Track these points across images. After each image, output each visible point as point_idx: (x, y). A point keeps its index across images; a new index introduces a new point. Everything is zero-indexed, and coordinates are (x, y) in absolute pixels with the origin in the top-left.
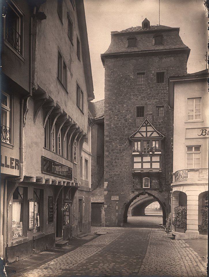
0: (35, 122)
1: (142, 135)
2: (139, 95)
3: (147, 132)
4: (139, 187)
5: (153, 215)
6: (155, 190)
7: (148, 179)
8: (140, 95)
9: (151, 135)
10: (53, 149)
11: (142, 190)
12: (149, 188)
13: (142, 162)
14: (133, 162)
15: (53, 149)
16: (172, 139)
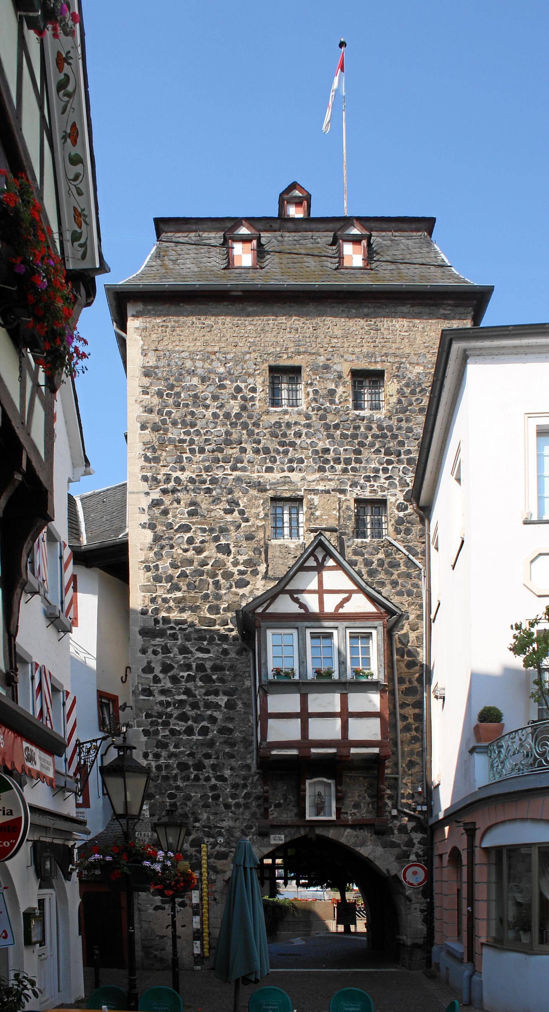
0: (439, 785)
1: (302, 606)
4: (288, 816)
6: (357, 826)
7: (329, 785)
8: (286, 453)
9: (341, 605)
11: (305, 826)
12: (334, 817)
16: (98, 872)
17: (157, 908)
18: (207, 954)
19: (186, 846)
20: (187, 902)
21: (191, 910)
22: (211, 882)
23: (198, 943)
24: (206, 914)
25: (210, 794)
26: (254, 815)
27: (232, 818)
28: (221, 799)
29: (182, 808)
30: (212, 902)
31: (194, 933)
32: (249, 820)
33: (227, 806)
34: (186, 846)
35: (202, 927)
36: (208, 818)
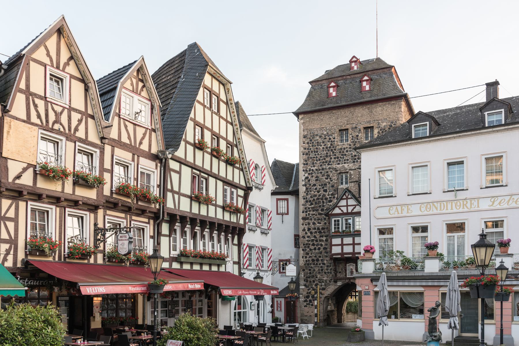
1: (342, 211)
2: (341, 157)
3: (347, 206)
5: (107, 89)
8: (343, 158)
9: (353, 210)
10: (182, 133)
13: (342, 245)
14: (331, 245)
15: (182, 133)
17: (305, 306)
19: (314, 286)
22: (320, 298)
26: (333, 275)
33: (325, 273)
34: (314, 286)
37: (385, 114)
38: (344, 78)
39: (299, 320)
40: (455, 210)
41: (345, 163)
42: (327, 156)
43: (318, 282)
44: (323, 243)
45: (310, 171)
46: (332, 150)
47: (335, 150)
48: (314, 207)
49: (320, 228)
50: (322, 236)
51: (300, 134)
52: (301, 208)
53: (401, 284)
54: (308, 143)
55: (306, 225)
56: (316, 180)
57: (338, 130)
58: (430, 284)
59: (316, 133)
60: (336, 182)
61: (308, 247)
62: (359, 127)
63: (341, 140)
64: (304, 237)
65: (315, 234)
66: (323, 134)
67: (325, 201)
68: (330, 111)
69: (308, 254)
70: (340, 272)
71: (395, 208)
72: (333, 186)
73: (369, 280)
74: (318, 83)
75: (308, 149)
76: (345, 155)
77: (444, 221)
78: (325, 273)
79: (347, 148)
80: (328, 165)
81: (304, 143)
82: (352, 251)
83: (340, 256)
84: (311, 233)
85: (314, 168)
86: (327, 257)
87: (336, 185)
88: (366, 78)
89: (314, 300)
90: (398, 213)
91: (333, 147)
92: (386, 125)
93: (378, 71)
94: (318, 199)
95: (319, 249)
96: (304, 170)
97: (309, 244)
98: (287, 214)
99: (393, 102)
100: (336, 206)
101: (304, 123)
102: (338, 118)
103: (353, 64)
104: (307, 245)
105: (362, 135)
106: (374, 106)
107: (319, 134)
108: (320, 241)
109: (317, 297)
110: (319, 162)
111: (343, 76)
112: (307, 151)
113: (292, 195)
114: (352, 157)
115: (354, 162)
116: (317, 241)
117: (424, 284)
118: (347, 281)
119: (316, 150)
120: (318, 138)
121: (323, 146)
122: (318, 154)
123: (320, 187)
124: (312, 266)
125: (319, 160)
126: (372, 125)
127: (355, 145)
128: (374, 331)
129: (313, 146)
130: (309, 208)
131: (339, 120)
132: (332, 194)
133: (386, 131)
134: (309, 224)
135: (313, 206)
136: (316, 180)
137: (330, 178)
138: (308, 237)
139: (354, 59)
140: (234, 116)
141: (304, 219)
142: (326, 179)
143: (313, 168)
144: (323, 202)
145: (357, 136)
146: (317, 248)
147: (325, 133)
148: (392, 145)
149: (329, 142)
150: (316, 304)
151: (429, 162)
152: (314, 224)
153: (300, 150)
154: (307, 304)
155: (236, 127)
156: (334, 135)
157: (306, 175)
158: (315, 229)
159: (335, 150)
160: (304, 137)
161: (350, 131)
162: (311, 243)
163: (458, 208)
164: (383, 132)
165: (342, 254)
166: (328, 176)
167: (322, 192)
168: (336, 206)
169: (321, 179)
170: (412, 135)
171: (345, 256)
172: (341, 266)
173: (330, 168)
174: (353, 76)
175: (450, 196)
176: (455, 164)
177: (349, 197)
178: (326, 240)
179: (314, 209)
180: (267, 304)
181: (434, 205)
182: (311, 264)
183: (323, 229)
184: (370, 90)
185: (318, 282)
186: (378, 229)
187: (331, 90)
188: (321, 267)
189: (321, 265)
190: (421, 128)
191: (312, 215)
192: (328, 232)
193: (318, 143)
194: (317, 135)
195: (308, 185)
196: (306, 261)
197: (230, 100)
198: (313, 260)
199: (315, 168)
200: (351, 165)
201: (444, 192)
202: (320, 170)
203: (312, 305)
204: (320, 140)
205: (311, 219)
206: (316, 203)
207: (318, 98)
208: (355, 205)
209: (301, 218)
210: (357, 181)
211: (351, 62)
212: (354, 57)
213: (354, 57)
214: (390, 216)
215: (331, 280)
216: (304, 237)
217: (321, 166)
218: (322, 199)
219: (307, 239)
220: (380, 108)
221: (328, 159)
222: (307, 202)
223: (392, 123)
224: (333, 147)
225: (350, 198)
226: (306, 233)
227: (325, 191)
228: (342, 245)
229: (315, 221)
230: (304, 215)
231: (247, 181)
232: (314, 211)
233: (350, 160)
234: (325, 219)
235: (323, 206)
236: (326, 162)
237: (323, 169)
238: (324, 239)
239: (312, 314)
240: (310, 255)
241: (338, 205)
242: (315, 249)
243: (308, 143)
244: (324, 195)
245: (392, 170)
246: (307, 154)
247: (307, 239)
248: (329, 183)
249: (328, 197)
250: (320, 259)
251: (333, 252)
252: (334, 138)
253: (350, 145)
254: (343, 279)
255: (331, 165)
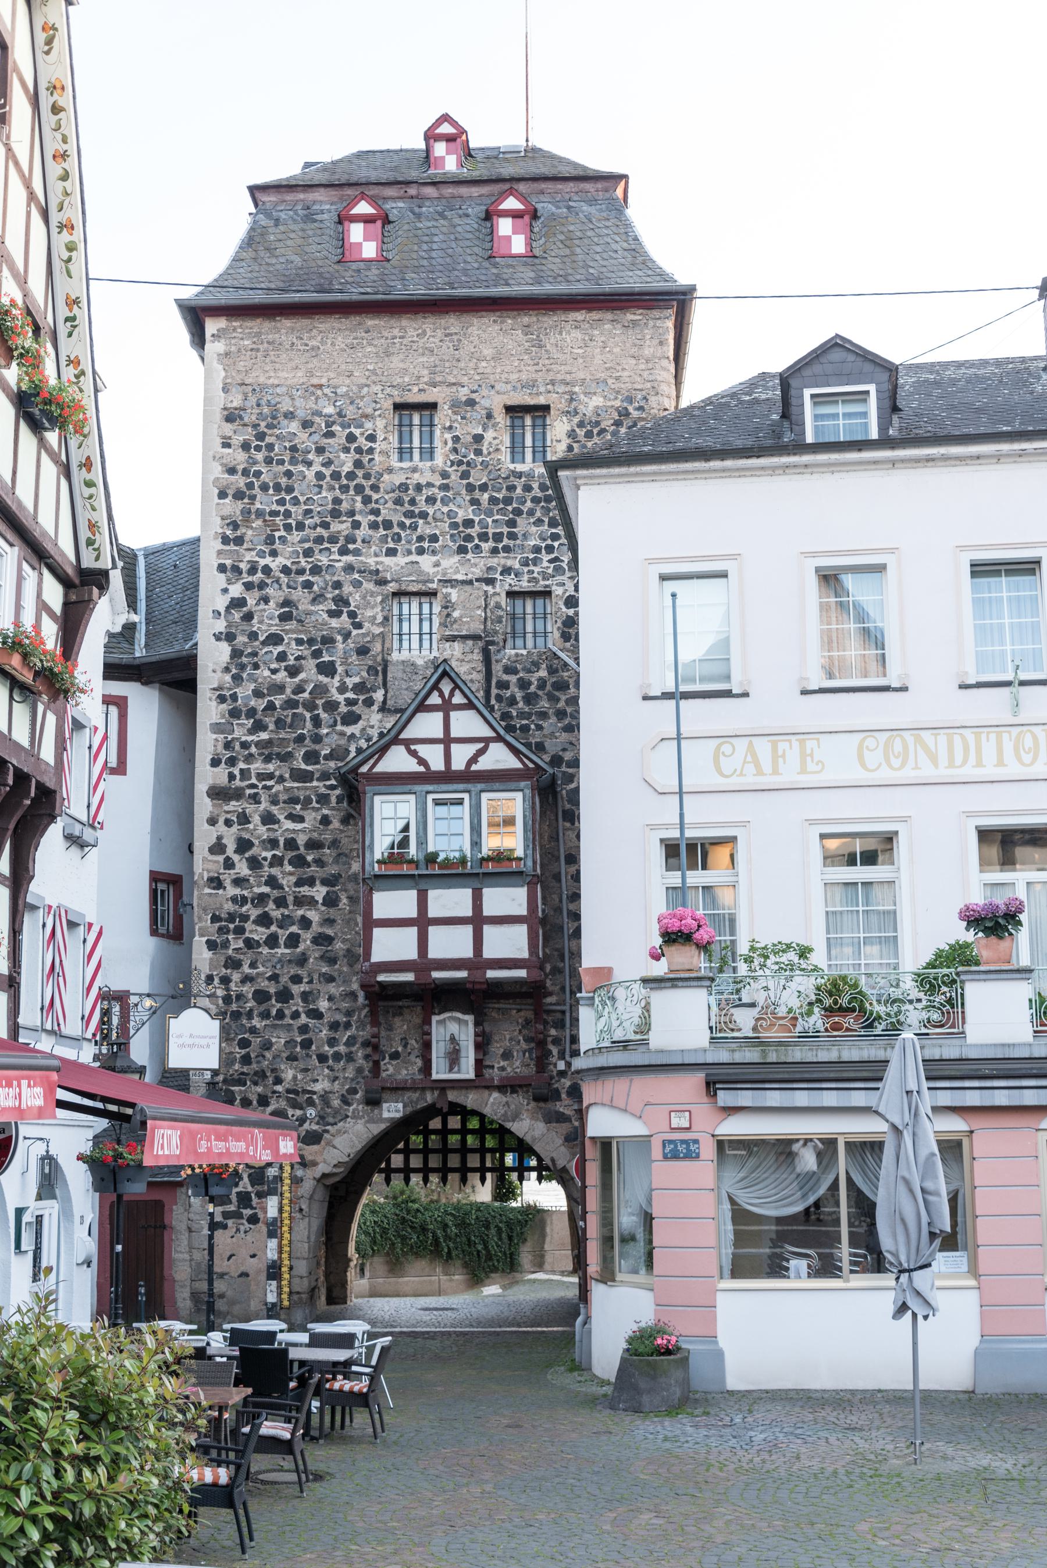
1: (422, 762)
2: (402, 525)
3: (447, 741)
8: (414, 527)
9: (474, 760)
13: (422, 922)
14: (371, 923)
18: (286, 1303)
20: (261, 1215)
21: (264, 1229)
22: (296, 1181)
23: (274, 1283)
24: (287, 1235)
25: (299, 1040)
26: (359, 1070)
27: (328, 1076)
28: (313, 1047)
29: (258, 1062)
30: (298, 1215)
31: (269, 1267)
32: (352, 1080)
33: (322, 1058)
35: (280, 1258)
36: (295, 1078)
37: (598, 361)
38: (412, 191)
39: (183, 1299)
40: (1014, 770)
41: (421, 551)
42: (335, 514)
43: (283, 1104)
44: (313, 915)
45: (252, 570)
46: (360, 489)
47: (375, 488)
48: (269, 743)
49: (302, 839)
50: (311, 882)
51: (208, 400)
52: (207, 743)
53: (830, 1098)
54: (246, 446)
55: (228, 823)
56: (285, 618)
57: (388, 405)
58: (1001, 1098)
59: (286, 406)
60: (377, 630)
61: (240, 931)
62: (486, 403)
63: (401, 451)
64: (216, 883)
65: (275, 871)
66: (318, 413)
67: (324, 716)
68: (355, 319)
69: (234, 964)
70: (395, 1056)
71: (741, 744)
72: (363, 651)
73: (698, 1078)
74: (290, 197)
75: (245, 473)
76: (424, 515)
77: (970, 814)
78: (322, 1058)
79: (430, 485)
80: (343, 551)
81: (226, 445)
82: (468, 952)
83: (409, 977)
84: (254, 863)
85: (275, 564)
86: (330, 979)
87: (377, 648)
88: (512, 203)
89: (260, 1195)
90: (760, 772)
91: (367, 476)
92: (606, 409)
93: (560, 186)
94: (291, 704)
95: (293, 941)
96: (222, 568)
97: (245, 918)
98: (120, 769)
99: (630, 317)
100: (396, 741)
101: (227, 354)
102: (388, 354)
103: (440, 149)
104: (229, 923)
105: (498, 437)
106: (550, 320)
107: (300, 413)
108: (301, 901)
109: (279, 1179)
110: (296, 536)
111: (408, 183)
112: (240, 481)
113: (145, 683)
114: (454, 525)
115: (462, 550)
116: (281, 902)
117: (973, 1099)
118: (430, 1098)
119: (284, 481)
120: (294, 426)
121: (316, 467)
122: (296, 501)
123: (305, 651)
124: (256, 1022)
125: (300, 526)
126: (542, 400)
127: (465, 475)
128: (723, 1342)
129: (268, 461)
130: (245, 745)
131: (396, 363)
132: (360, 688)
133: (603, 431)
134: (244, 819)
135: (264, 736)
136: (285, 618)
137: (352, 615)
138: (238, 882)
139: (446, 129)
140: (65, 177)
141: (217, 794)
142: (334, 614)
143: (267, 560)
144: (317, 721)
145: (478, 439)
146: (283, 935)
147: (330, 410)
148: (729, 463)
149: (347, 450)
150: (272, 1212)
151: (892, 551)
152: (268, 819)
153: (205, 472)
154: (226, 1215)
155: (65, 237)
156: (368, 425)
157: (237, 590)
158: (273, 843)
159: (375, 488)
160: (229, 419)
161: (443, 416)
162: (254, 913)
163: (1027, 758)
164: (589, 435)
165: (423, 964)
166: (342, 601)
167: (310, 673)
168: (391, 740)
169: (309, 613)
170: (803, 433)
171: (436, 974)
172: (401, 1026)
173: (349, 568)
174: (449, 191)
175: (993, 705)
176: (997, 573)
177: (458, 699)
178: (331, 901)
179: (269, 751)
180: (77, 1220)
181: (919, 740)
182: (250, 1015)
183: (313, 845)
184: (530, 255)
185: (283, 1104)
186: (662, 840)
187: (356, 232)
188: (304, 1029)
189: (303, 1019)
190: (840, 409)
191: (261, 777)
192: (336, 860)
193: (294, 449)
194: (290, 416)
195: (242, 639)
196: (227, 999)
197: (52, 88)
198: (261, 996)
199: (281, 561)
200: (450, 564)
201: (963, 687)
202: (301, 572)
203: (253, 1220)
204: (304, 440)
205: (255, 799)
206: (280, 723)
207: (297, 260)
208: (487, 741)
209: (201, 788)
210: (475, 637)
211: (431, 136)
212: (445, 118)
213: (445, 118)
214: (721, 783)
215: (353, 1091)
216: (216, 883)
217: (308, 553)
218: (310, 706)
219: (232, 891)
220: (577, 334)
221: (341, 527)
222: (235, 713)
223: (630, 400)
224: (367, 476)
225: (460, 707)
226: (229, 864)
227: (327, 669)
228: (422, 922)
229: (275, 810)
230: (220, 776)
231: (84, 534)
232: (268, 759)
233: (444, 540)
234: (323, 799)
235: (317, 739)
236: (333, 539)
237: (316, 570)
238: (319, 892)
239: (253, 1266)
240: (246, 969)
241: (402, 736)
242: (272, 941)
243: (246, 446)
244: (320, 690)
245: (724, 575)
246: (239, 495)
247: (232, 891)
248: (347, 636)
249: (341, 698)
250: (296, 989)
251: (376, 957)
252: (372, 438)
253: (445, 475)
254: (414, 1089)
255: (357, 553)
